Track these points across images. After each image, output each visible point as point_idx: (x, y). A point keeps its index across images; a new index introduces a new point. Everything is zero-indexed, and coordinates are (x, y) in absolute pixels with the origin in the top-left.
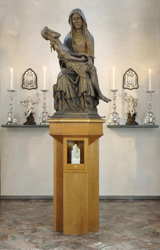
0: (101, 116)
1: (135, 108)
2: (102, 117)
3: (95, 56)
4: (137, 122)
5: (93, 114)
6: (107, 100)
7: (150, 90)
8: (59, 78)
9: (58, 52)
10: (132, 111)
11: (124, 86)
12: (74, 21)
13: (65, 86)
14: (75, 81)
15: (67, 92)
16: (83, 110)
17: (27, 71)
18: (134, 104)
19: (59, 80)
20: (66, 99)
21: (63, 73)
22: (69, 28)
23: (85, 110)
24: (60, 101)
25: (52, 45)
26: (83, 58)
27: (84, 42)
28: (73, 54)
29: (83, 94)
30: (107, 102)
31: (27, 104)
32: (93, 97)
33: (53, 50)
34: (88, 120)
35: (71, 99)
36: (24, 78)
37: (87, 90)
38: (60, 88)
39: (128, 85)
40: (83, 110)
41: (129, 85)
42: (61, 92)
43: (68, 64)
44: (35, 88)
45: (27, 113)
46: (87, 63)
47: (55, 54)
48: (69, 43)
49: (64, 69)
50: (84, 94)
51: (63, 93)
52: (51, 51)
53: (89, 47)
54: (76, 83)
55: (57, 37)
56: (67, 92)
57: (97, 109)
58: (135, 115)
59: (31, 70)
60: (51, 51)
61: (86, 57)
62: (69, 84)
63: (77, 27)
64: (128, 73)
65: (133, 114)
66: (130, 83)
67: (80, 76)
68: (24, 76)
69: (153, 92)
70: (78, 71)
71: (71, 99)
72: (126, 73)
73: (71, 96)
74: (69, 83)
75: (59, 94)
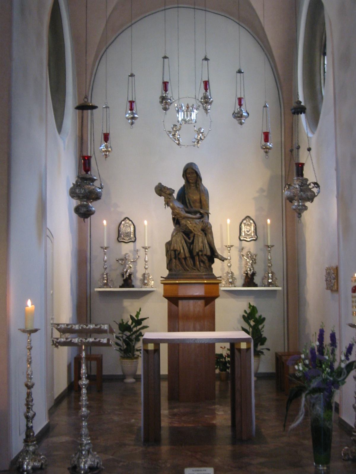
0: (217, 275)
1: (254, 266)
2: (218, 277)
3: (210, 212)
4: (256, 283)
5: (209, 274)
6: (223, 259)
7: (269, 244)
8: (173, 236)
9: (173, 208)
10: (250, 270)
11: (240, 237)
12: (188, 176)
13: (181, 245)
14: (189, 239)
15: (182, 251)
16: (198, 269)
17: (123, 220)
18: (253, 261)
19: (174, 238)
20: (179, 259)
21: (176, 231)
22: (182, 182)
23: (200, 268)
24: (174, 260)
25: (167, 202)
26: (198, 215)
27: (199, 197)
28: (186, 209)
29: (198, 254)
30: (223, 261)
31: (125, 262)
32: (208, 256)
33: (167, 206)
34: (204, 280)
35: (185, 258)
36: (120, 229)
37: (203, 248)
38: (174, 247)
39: (244, 236)
40: (198, 269)
41: (246, 236)
42: (175, 251)
43: (183, 222)
44: (134, 240)
45: (124, 273)
46: (202, 220)
47: (169, 210)
48: (183, 196)
49: (178, 226)
50: (200, 253)
51: (177, 253)
52: (165, 208)
53: (204, 203)
54: (191, 241)
55: (171, 193)
56: (182, 251)
57: (212, 269)
58: (254, 274)
59: (128, 219)
60: (165, 208)
61: (201, 214)
62: (184, 243)
63: (191, 181)
64: (245, 222)
65: (250, 274)
66: (248, 233)
67: (194, 234)
68: (120, 227)
69: (272, 246)
70: (194, 230)
71: (185, 258)
72: (242, 222)
73: (185, 255)
74: (183, 241)
75: (173, 253)
